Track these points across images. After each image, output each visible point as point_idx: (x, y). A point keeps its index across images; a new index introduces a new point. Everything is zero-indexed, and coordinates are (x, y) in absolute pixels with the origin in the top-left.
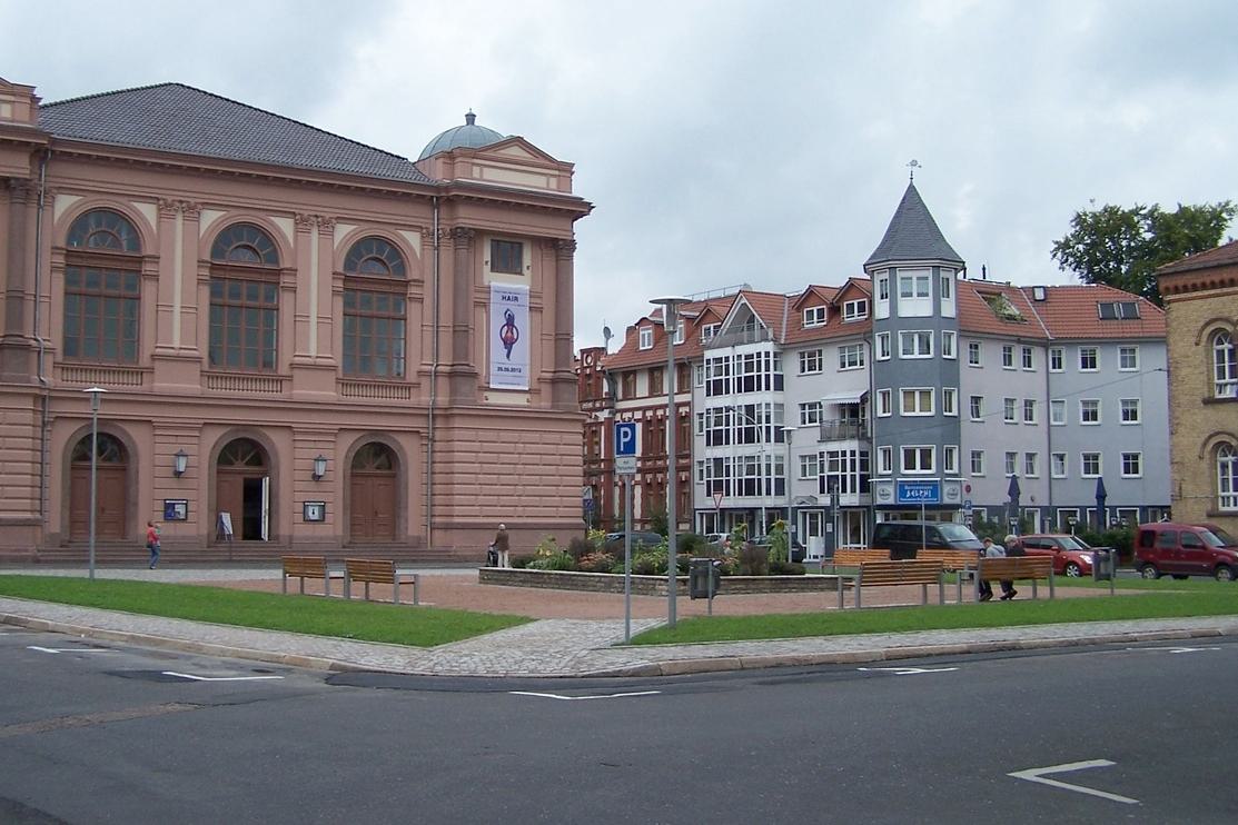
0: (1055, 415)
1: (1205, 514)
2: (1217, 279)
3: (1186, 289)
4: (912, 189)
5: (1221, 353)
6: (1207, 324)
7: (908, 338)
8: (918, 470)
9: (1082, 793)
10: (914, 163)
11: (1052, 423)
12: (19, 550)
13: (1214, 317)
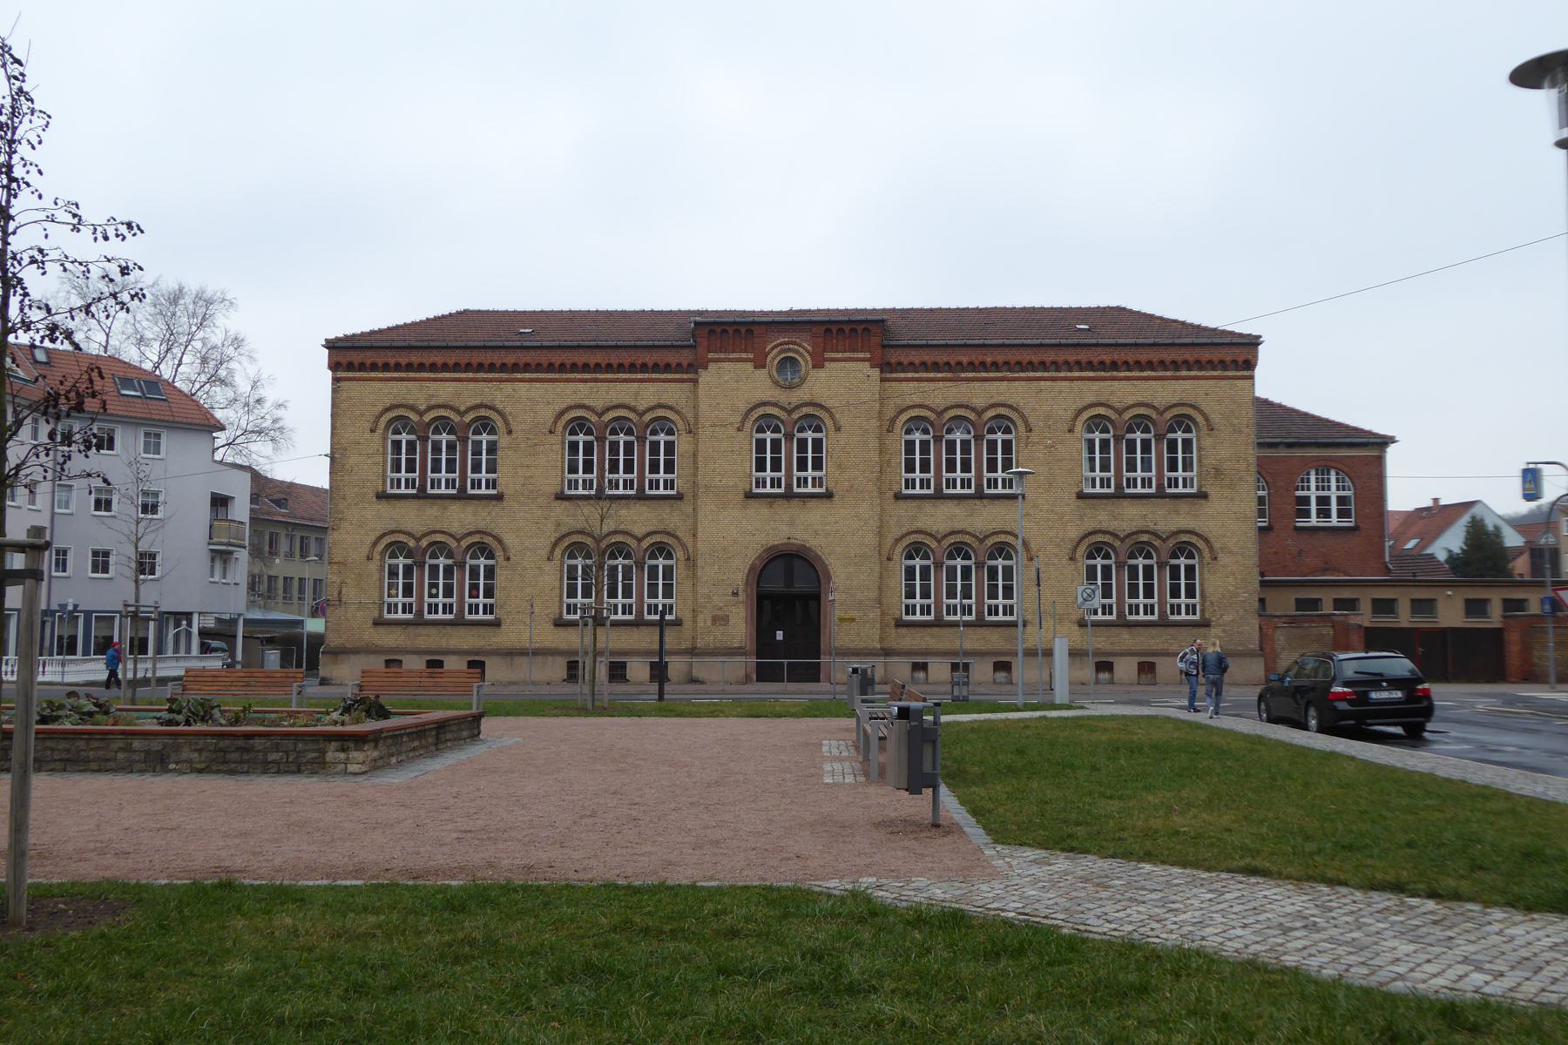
0: (59, 501)
2: (404, 361)
5: (397, 444)
6: (387, 410)
11: (57, 510)
12: (311, 520)
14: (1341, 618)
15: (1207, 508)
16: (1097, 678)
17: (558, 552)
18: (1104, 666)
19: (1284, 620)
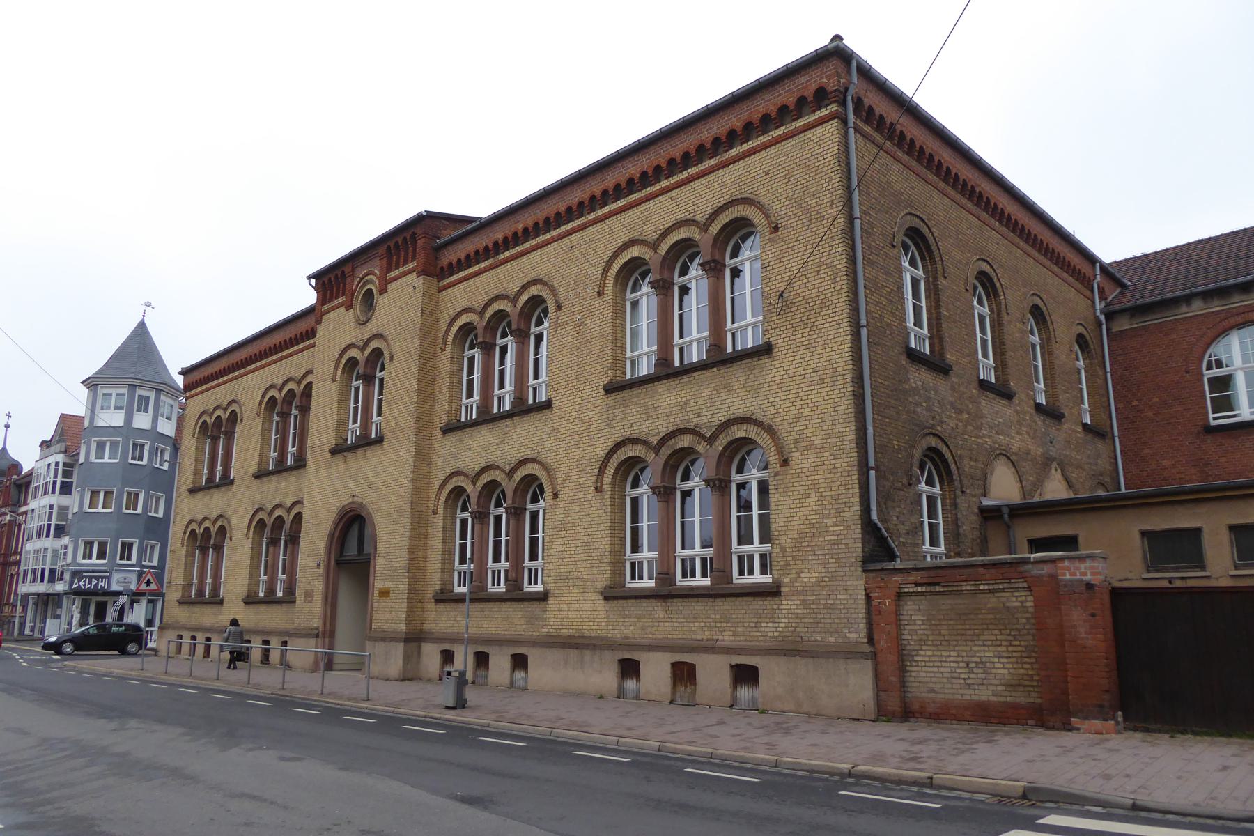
4: (142, 325)
7: (101, 446)
8: (94, 560)
9: (1109, 349)
10: (148, 304)
14: (1046, 569)
15: (774, 370)
16: (734, 699)
17: (608, 478)
18: (629, 669)
19: (914, 577)
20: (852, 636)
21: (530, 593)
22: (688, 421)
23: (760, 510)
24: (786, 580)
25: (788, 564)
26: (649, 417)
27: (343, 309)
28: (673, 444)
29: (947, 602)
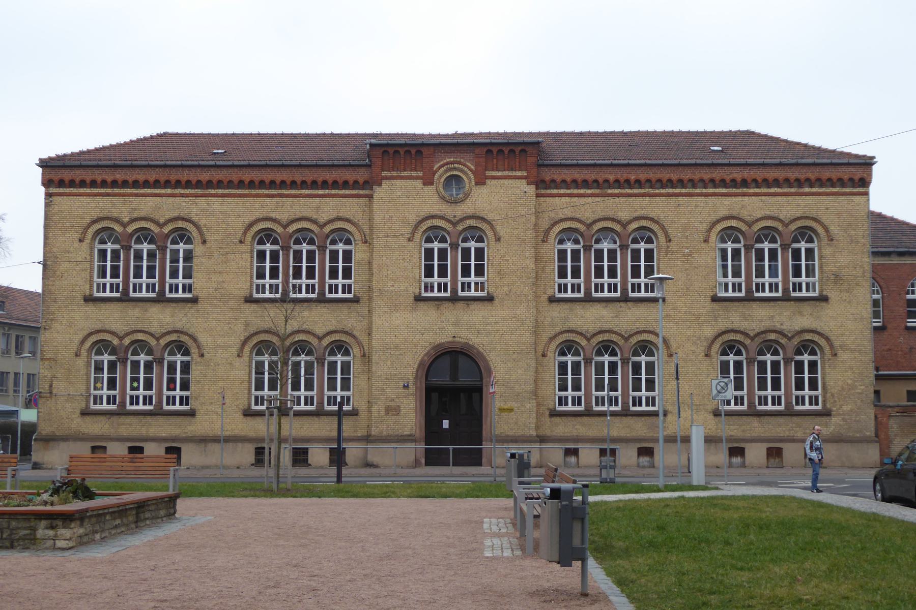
1: (78, 412)
2: (109, 178)
3: (72, 183)
6: (94, 222)
13: (101, 215)
15: (828, 310)
17: (247, 349)
19: (897, 409)
20: (868, 434)
21: (328, 411)
22: (774, 326)
23: (804, 377)
24: (834, 409)
25: (835, 401)
26: (746, 320)
27: (524, 181)
28: (764, 337)
29: (908, 420)
